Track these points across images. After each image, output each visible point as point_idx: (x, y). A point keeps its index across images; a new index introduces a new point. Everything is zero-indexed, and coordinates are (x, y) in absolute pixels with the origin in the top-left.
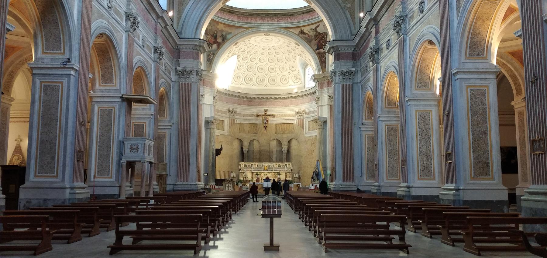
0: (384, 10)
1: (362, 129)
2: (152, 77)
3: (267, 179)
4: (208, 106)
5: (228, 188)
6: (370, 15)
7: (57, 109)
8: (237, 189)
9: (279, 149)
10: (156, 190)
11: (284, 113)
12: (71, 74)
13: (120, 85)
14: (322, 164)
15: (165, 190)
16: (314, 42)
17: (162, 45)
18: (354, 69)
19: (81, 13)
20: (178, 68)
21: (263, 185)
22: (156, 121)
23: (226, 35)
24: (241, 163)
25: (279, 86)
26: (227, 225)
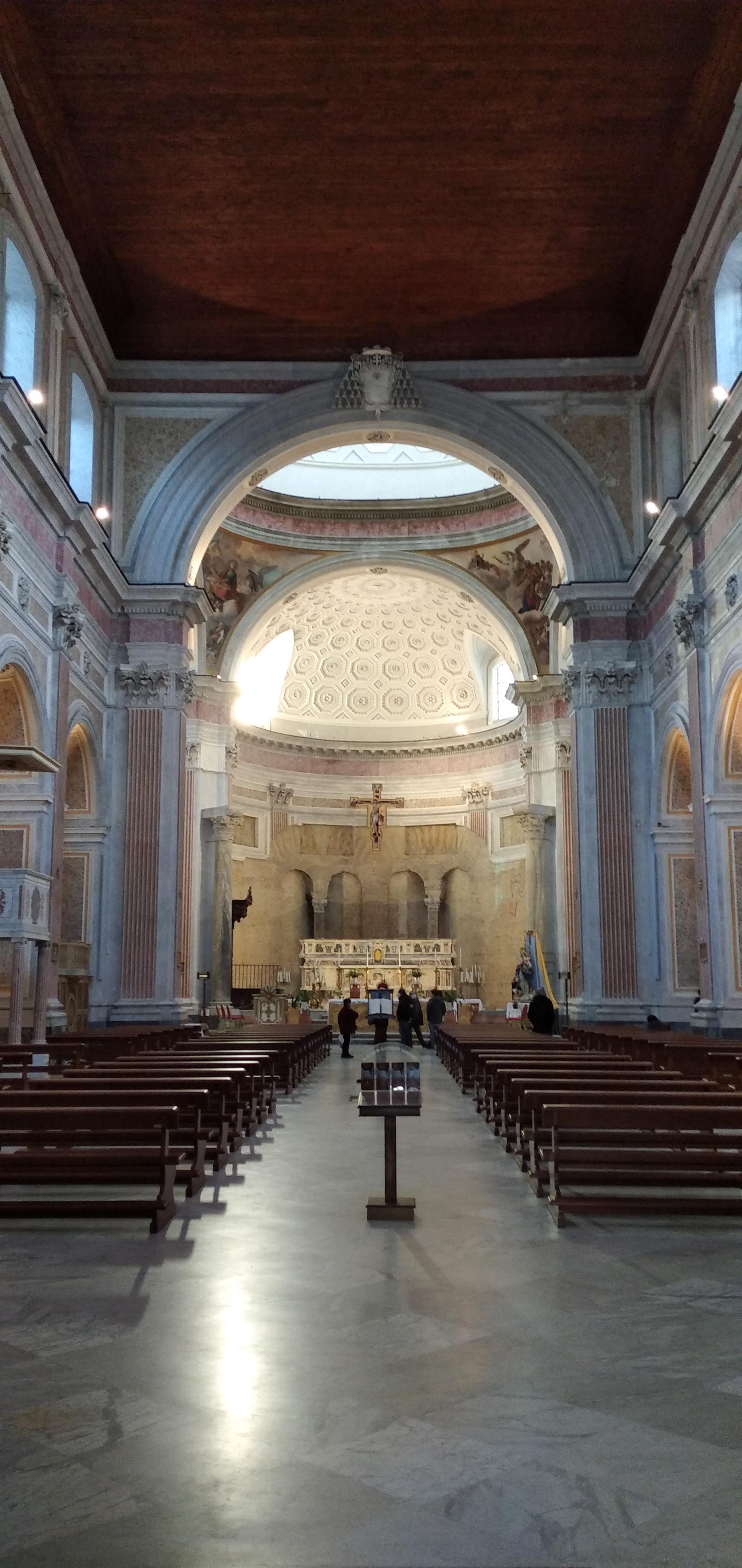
0: (717, 491)
1: (658, 840)
2: (49, 693)
3: (383, 991)
4: (211, 776)
5: (267, 1015)
6: (675, 506)
8: (294, 1020)
9: (415, 899)
10: (56, 1024)
11: (430, 796)
14: (543, 943)
16: (515, 590)
17: (79, 602)
18: (631, 665)
20: (124, 668)
21: (367, 1005)
22: (59, 819)
24: (306, 942)
25: (414, 716)
26: (259, 1134)
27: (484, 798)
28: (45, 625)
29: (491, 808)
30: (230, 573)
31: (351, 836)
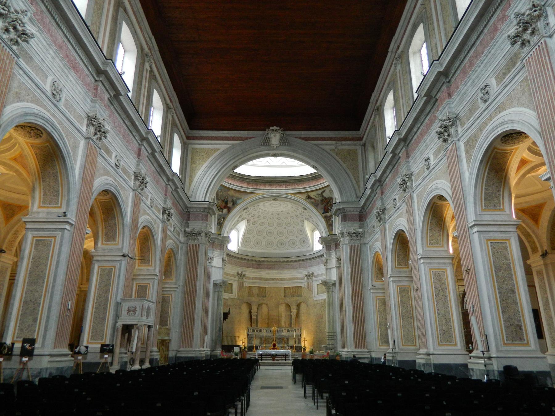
2: (159, 238)
4: (217, 268)
7: (46, 265)
12: (65, 229)
13: (123, 244)
15: (167, 358)
16: (321, 206)
18: (361, 230)
19: (84, 168)
20: (187, 230)
28: (130, 180)
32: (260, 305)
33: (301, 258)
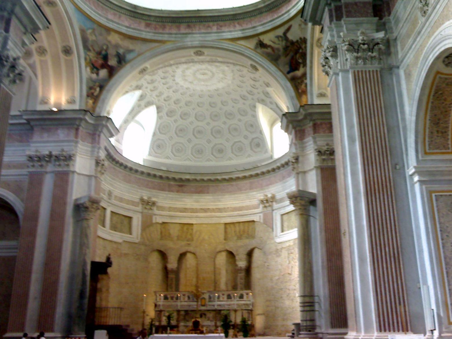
16: (284, 60)
18: (381, 35)
23: (124, 53)
25: (230, 159)
27: (270, 203)
29: (276, 209)
30: (104, 52)
31: (192, 229)
32: (182, 256)
33: (253, 173)
